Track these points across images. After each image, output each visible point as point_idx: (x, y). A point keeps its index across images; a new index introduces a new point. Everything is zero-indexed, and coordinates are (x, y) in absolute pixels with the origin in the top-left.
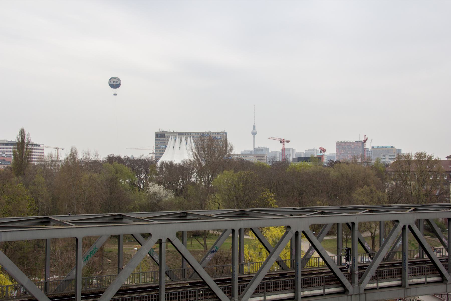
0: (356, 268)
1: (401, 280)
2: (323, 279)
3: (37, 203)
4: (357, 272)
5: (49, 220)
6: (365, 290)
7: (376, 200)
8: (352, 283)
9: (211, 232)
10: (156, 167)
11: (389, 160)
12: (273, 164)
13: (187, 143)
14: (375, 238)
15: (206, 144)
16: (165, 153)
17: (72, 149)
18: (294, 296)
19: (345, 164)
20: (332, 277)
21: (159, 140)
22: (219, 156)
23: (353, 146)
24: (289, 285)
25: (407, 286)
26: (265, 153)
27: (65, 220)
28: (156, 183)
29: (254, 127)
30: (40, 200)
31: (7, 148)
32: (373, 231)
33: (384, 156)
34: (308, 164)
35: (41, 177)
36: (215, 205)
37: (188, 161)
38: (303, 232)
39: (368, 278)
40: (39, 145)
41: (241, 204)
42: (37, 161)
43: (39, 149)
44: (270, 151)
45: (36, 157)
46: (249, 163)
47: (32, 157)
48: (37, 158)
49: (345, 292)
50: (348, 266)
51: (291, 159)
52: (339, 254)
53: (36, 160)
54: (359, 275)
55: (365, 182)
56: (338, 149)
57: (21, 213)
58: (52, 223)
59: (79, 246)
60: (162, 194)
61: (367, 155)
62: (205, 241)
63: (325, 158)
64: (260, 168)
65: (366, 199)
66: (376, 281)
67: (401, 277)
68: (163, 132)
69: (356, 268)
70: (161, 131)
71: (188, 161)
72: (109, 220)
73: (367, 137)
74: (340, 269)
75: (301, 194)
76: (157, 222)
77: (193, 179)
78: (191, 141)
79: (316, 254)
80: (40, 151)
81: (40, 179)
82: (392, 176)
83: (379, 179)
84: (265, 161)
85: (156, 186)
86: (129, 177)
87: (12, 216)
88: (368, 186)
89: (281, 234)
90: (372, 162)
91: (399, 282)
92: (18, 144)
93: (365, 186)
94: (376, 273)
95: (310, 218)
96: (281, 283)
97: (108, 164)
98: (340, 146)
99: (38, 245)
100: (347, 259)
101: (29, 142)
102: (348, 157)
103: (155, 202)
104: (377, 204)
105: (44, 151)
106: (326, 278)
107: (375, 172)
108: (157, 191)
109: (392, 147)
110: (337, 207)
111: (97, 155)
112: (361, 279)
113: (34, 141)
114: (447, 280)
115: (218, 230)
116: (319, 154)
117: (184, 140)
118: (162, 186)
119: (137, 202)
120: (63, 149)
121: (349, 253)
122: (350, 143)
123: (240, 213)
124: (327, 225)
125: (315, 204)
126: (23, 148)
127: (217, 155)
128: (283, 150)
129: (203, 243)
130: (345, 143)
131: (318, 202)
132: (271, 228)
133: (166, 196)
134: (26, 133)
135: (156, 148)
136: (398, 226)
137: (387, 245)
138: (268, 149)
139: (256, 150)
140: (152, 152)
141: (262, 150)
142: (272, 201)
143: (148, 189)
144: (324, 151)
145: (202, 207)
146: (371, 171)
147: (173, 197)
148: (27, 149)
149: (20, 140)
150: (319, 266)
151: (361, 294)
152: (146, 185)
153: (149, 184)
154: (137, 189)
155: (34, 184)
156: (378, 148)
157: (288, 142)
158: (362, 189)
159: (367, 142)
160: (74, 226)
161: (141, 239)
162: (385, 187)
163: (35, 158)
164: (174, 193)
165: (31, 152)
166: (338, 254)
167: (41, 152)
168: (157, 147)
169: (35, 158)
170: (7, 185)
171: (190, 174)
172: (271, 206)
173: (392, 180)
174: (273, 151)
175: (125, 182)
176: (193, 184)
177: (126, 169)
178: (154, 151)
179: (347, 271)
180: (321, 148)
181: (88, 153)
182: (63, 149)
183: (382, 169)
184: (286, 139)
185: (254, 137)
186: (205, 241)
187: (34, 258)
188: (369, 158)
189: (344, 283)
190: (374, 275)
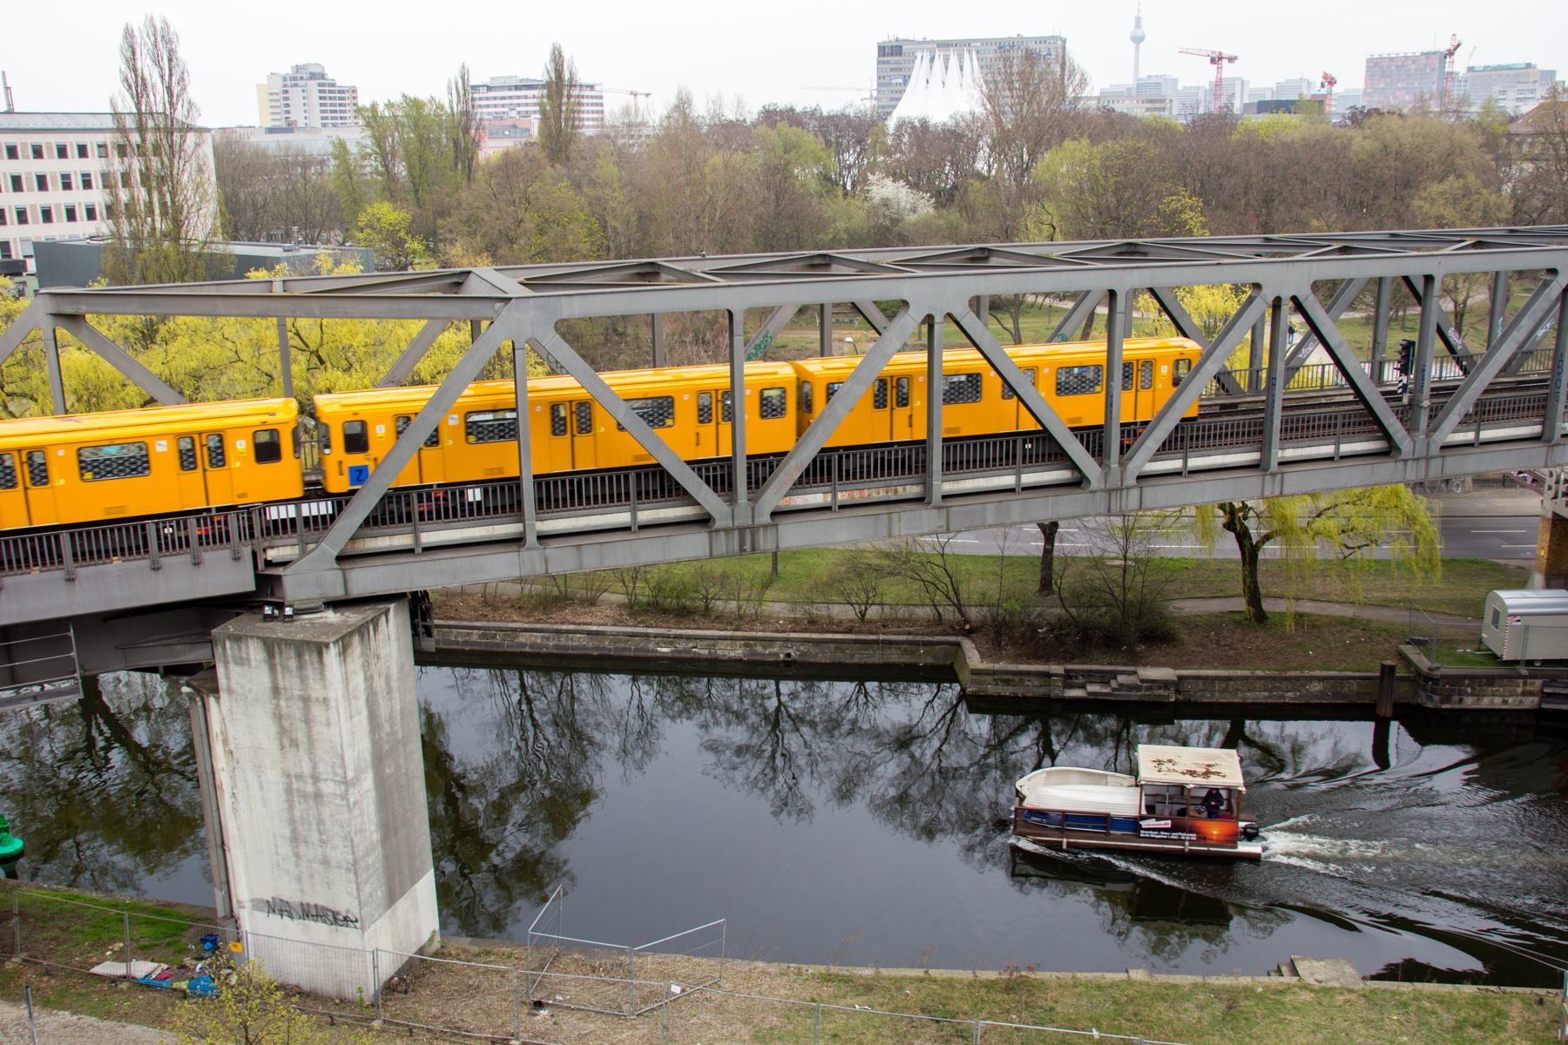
0: (1426, 392)
1: (1543, 423)
2: (1336, 418)
3: (604, 227)
4: (1426, 403)
5: (656, 269)
6: (1140, 478)
7: (1476, 215)
8: (1411, 428)
9: (1030, 299)
10: (885, 134)
11: (1522, 104)
12: (1194, 122)
13: (961, 68)
14: (1466, 316)
15: (1015, 69)
16: (905, 97)
17: (680, 93)
18: (1260, 460)
19: (1395, 117)
20: (1361, 416)
21: (888, 62)
22: (1050, 101)
23: (1413, 67)
24: (1249, 432)
25: (1557, 437)
26: (1166, 92)
27: (698, 267)
28: (887, 176)
29: (1138, 21)
30: (612, 222)
31: (518, 97)
32: (1461, 298)
33: (1504, 92)
34: (1285, 117)
35: (611, 166)
36: (1040, 231)
37: (969, 118)
38: (1294, 299)
39: (1454, 417)
40: (592, 87)
41: (1109, 228)
42: (593, 127)
43: (592, 97)
44: (1180, 87)
45: (591, 116)
46: (1126, 119)
47: (582, 116)
48: (593, 119)
49: (1390, 450)
50: (1405, 387)
51: (1237, 107)
52: (1378, 358)
53: (591, 123)
54: (1431, 410)
55: (1448, 166)
56: (1370, 77)
57: (571, 254)
58: (664, 276)
59: (735, 332)
60: (903, 204)
61: (1456, 92)
62: (1016, 323)
63: (1333, 103)
64: (1160, 133)
65: (1449, 213)
66: (1474, 426)
67: (1543, 416)
68: (897, 40)
69: (1426, 392)
70: (892, 38)
71: (969, 118)
72: (803, 268)
73: (1458, 39)
74: (1383, 393)
75: (1267, 201)
76: (920, 273)
77: (980, 165)
78: (972, 64)
79: (1318, 355)
80: (595, 101)
81: (607, 169)
82: (1525, 148)
83: (1490, 156)
84: (1166, 113)
85: (889, 182)
86: (817, 160)
87: (551, 260)
88: (1458, 177)
89: (1232, 307)
90: (1473, 109)
91: (1537, 429)
92: (548, 85)
93: (1451, 178)
94: (1476, 405)
95: (1315, 264)
96: (1209, 429)
97: (763, 129)
98: (1378, 68)
99: (615, 330)
100: (1404, 370)
101: (571, 79)
102: (1400, 98)
103: (888, 223)
104: (1480, 225)
105: (603, 101)
106: (1344, 417)
107: (1480, 139)
108: (891, 196)
109: (1529, 66)
110: (1383, 233)
111: (739, 105)
112: (1434, 422)
113: (583, 77)
114: (1398, 449)
115: (1047, 295)
116: (1316, 90)
117: (954, 61)
118: (902, 183)
119: (841, 224)
120: (647, 95)
121: (1409, 357)
122: (1407, 58)
123: (1123, 249)
124: (1351, 281)
125: (1304, 226)
126: (560, 95)
127: (1045, 99)
128: (1218, 83)
129: (1010, 326)
130: (1392, 59)
131: (1315, 223)
132: (1196, 288)
133: (914, 210)
134: (566, 55)
135: (879, 85)
136: (1554, 285)
137: (1515, 333)
138: (1176, 81)
139: (1141, 86)
140: (868, 96)
141: (1159, 84)
142: (1193, 219)
143: (868, 191)
144: (1332, 82)
145: (1008, 235)
146: (1468, 137)
147: (931, 211)
148: (569, 96)
149: (553, 75)
150: (1322, 386)
151: (1433, 457)
152: (858, 182)
153: (870, 177)
154: (840, 192)
155: (593, 183)
156: (1486, 69)
157: (1231, 60)
158: (1441, 187)
159: (1457, 53)
160: (722, 282)
161: (877, 317)
162: (1501, 182)
163: (588, 119)
164: (933, 200)
165: (580, 104)
166: (1373, 357)
167: (597, 105)
168: (882, 82)
169: (588, 119)
170: (535, 186)
171: (973, 148)
172: (1190, 232)
173: (1527, 160)
174: (1188, 85)
175: (805, 175)
176: (978, 176)
177: (810, 140)
178: (875, 94)
179: (1400, 399)
180: (1326, 76)
181: (718, 102)
182: (647, 95)
183: (1500, 130)
184: (1226, 53)
185: (1137, 49)
186: (1016, 323)
187: (609, 360)
188: (1465, 101)
189: (1391, 430)
190: (1471, 410)
